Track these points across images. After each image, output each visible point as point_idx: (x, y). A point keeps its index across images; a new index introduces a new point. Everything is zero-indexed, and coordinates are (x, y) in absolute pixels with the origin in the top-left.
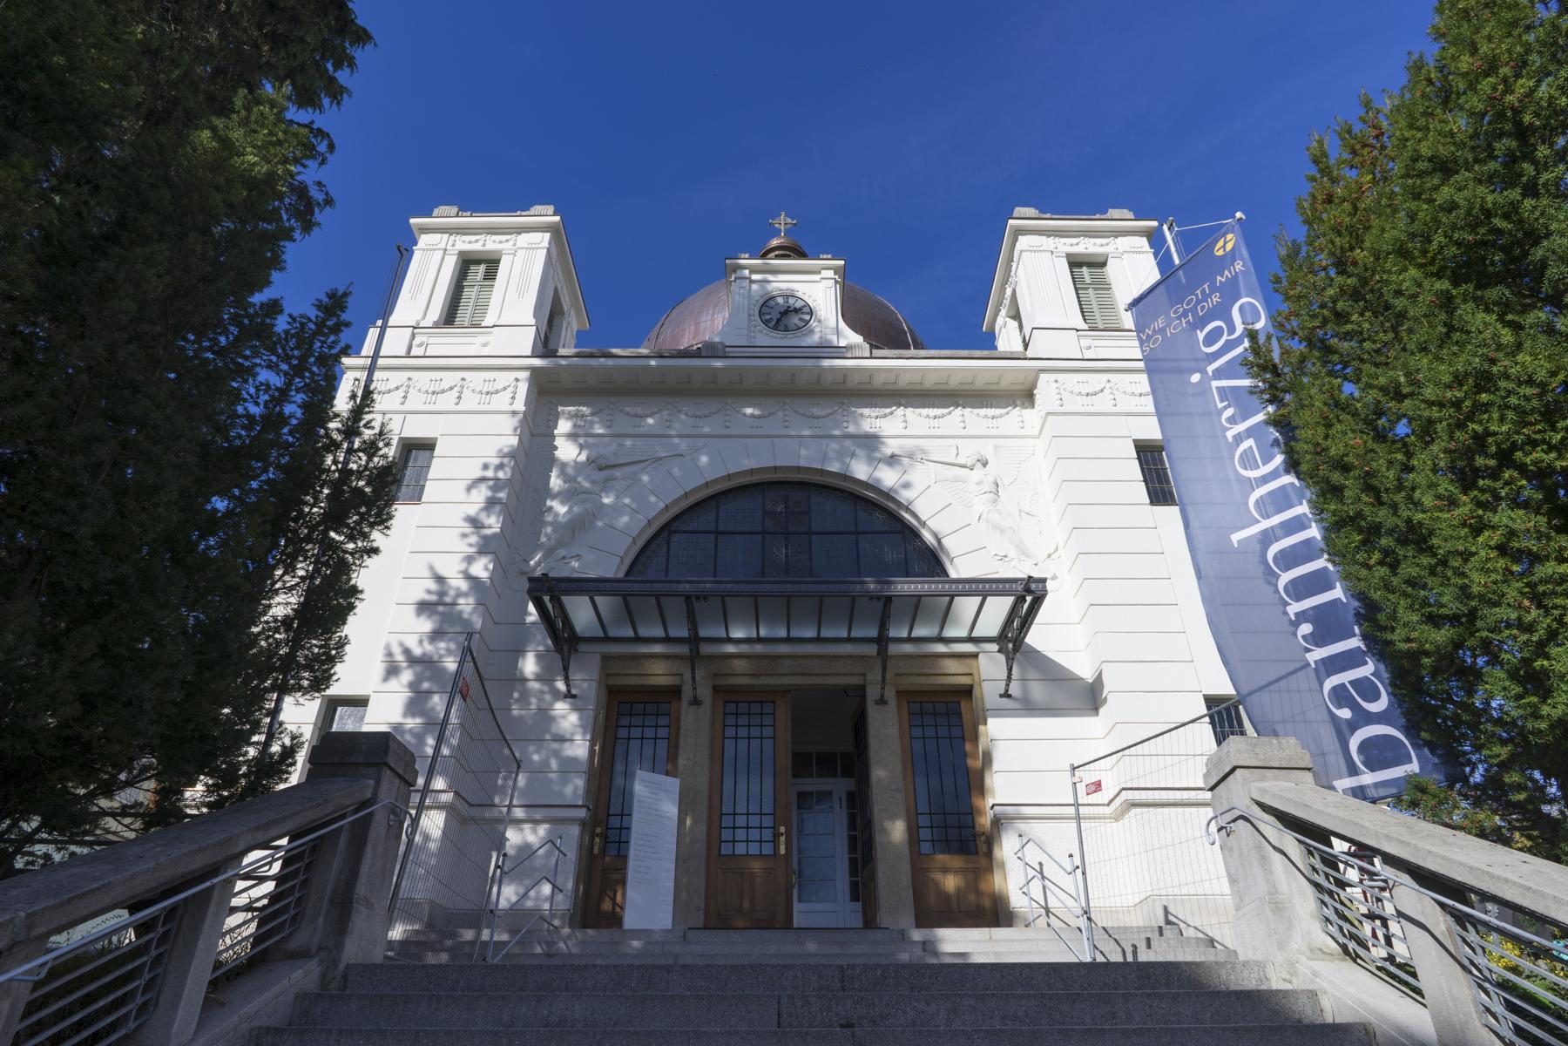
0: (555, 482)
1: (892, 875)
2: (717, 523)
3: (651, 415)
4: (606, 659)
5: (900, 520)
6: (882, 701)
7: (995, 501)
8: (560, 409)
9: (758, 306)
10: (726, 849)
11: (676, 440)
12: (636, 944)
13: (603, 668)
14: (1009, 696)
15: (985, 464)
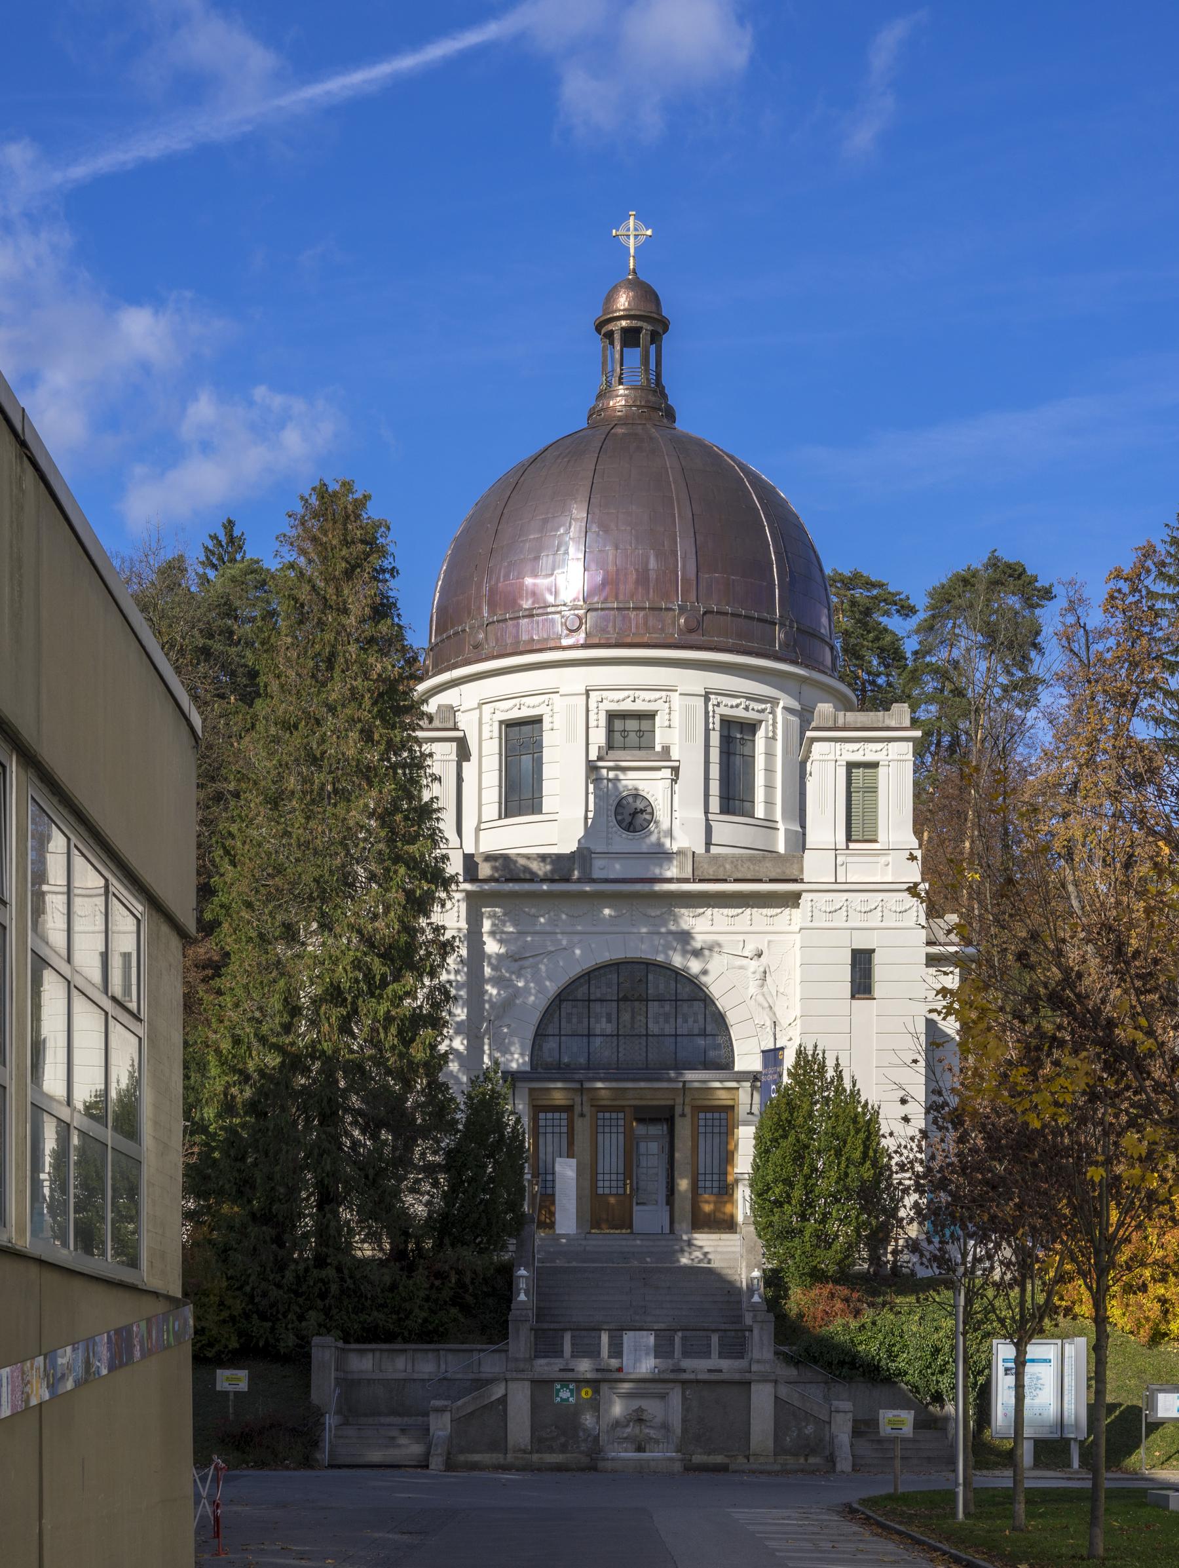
0: (488, 971)
1: (683, 1205)
2: (583, 1035)
3: (543, 916)
4: (531, 1090)
5: (702, 989)
6: (683, 1115)
7: (762, 986)
8: (483, 910)
9: (613, 808)
10: (600, 1191)
11: (559, 936)
12: (564, 1241)
13: (530, 1095)
14: (752, 1114)
15: (759, 955)
